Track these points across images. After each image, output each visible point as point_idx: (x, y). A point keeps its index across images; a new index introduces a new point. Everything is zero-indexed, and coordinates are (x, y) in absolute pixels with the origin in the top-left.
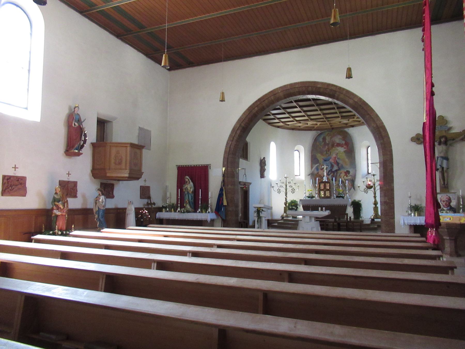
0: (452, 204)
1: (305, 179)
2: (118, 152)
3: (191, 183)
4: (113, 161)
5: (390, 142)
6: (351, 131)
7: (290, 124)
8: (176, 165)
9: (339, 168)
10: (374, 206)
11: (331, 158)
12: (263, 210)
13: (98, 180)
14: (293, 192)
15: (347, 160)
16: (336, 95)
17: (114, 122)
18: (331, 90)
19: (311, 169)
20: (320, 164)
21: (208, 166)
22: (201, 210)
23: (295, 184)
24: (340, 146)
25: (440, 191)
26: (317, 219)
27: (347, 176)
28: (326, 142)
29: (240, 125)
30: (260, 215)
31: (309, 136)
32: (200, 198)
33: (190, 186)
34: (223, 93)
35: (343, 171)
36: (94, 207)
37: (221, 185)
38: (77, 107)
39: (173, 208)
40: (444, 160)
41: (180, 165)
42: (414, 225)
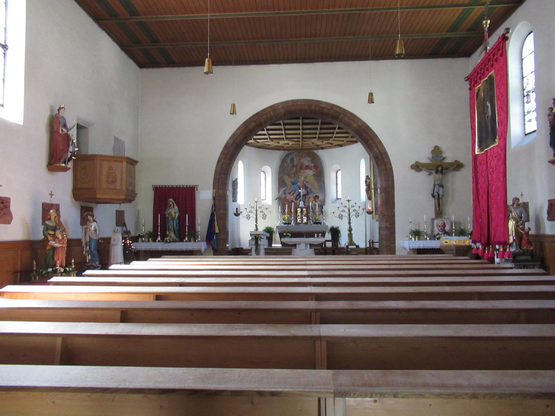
0: (446, 229)
1: (272, 204)
2: (110, 168)
3: (176, 207)
4: (104, 178)
5: (392, 168)
6: (321, 153)
7: (260, 142)
8: (152, 186)
9: (307, 192)
10: (349, 232)
11: (299, 182)
12: (262, 237)
13: (79, 202)
14: (264, 218)
15: (316, 184)
16: (340, 117)
17: (90, 128)
18: (336, 111)
19: (279, 193)
20: (287, 187)
21: (195, 187)
22: (188, 239)
23: (266, 209)
24: (309, 169)
25: (435, 217)
26: (311, 245)
27: (316, 201)
28: (294, 164)
29: (233, 142)
30: (258, 243)
31: (277, 156)
32: (187, 224)
33: (174, 211)
34: (234, 105)
35: (311, 196)
36: (82, 237)
37: (212, 210)
38: (62, 108)
39: (153, 236)
40: (440, 188)
41: (160, 185)
42: (417, 249)
